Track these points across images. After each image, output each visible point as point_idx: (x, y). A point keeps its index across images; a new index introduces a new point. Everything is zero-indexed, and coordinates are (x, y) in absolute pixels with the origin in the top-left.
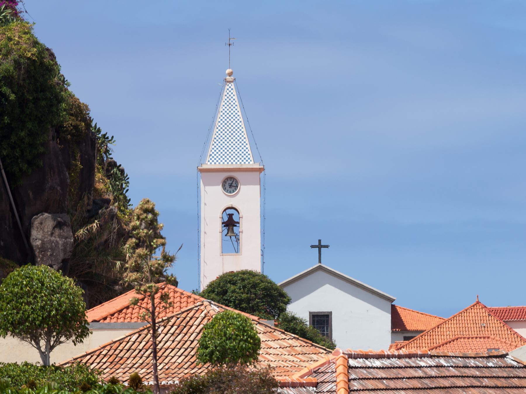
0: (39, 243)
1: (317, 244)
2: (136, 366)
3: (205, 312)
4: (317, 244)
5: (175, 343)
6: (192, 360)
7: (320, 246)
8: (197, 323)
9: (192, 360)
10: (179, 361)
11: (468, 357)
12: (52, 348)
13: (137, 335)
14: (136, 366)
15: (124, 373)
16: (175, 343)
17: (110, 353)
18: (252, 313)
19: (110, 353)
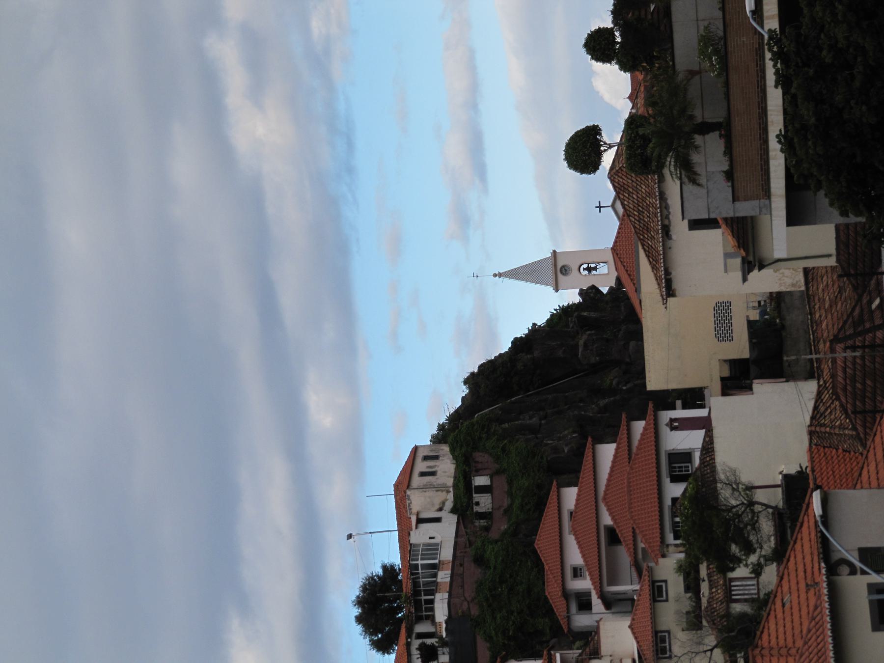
0: (597, 358)
1: (598, 209)
2: (648, 215)
3: (614, 176)
4: (598, 209)
5: (634, 192)
6: (643, 179)
7: (600, 207)
8: (621, 180)
9: (643, 179)
10: (644, 187)
11: (809, 526)
12: (605, 143)
13: (631, 218)
14: (648, 215)
15: (653, 221)
16: (634, 192)
17: (641, 233)
18: (729, 550)
19: (641, 233)
